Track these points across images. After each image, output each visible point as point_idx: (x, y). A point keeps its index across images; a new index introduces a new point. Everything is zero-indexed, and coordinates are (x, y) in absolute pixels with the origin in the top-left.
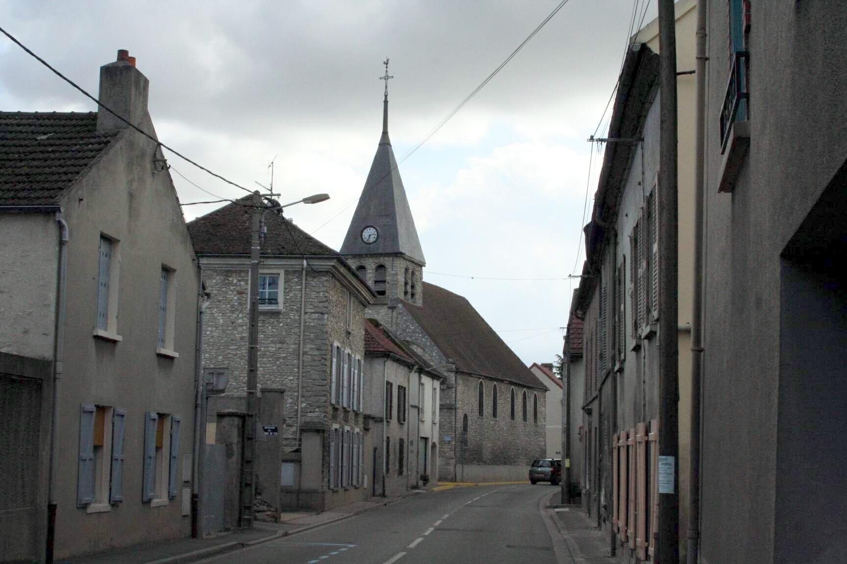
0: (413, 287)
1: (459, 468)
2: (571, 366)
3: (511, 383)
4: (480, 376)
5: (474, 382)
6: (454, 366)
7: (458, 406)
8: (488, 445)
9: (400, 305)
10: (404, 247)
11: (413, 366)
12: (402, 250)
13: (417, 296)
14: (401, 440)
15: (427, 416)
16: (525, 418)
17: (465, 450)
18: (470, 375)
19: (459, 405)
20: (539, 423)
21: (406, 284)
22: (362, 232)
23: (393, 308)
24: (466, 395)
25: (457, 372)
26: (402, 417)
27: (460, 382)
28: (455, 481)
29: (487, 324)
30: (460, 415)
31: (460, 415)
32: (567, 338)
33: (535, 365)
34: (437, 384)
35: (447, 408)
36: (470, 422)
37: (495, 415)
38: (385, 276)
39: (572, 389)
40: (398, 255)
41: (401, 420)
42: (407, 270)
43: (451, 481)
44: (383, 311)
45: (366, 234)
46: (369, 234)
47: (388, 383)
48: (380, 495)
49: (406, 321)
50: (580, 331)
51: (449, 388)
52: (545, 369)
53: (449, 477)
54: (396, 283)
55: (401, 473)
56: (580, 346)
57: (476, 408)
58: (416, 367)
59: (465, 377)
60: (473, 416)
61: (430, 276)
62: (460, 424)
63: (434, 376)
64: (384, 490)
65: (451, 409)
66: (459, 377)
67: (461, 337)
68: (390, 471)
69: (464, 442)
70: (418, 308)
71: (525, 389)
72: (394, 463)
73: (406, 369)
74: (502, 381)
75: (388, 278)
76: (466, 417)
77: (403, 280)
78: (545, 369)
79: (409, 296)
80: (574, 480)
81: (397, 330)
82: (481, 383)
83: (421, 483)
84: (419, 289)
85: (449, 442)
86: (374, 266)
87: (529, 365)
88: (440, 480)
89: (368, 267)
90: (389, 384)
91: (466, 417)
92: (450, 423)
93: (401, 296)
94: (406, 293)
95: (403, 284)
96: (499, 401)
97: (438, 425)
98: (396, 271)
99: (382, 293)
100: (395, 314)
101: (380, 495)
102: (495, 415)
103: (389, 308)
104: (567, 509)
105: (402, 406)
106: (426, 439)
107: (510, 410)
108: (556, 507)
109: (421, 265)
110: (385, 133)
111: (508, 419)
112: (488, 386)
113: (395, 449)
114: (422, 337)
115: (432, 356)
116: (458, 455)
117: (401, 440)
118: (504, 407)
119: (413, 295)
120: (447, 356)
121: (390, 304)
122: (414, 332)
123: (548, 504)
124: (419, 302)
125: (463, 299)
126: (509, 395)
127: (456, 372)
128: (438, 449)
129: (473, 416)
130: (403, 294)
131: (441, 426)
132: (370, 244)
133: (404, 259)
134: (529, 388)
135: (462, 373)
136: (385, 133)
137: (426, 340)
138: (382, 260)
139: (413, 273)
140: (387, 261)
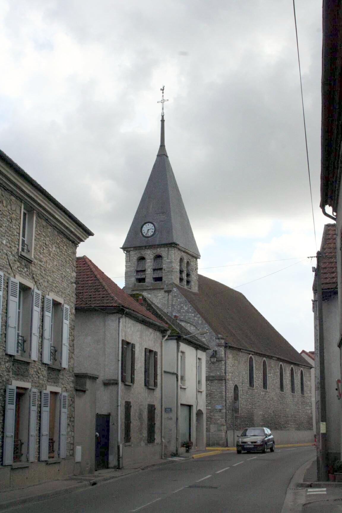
0: (188, 275)
1: (230, 433)
2: (325, 305)
3: (279, 360)
4: (249, 352)
5: (244, 358)
6: (223, 341)
7: (227, 377)
8: (259, 414)
9: (174, 289)
10: (177, 238)
11: (166, 330)
12: (175, 241)
13: (192, 283)
14: (151, 409)
15: (191, 382)
16: (293, 390)
17: (236, 418)
18: (239, 350)
19: (229, 376)
20: (306, 395)
21: (181, 272)
22: (142, 227)
23: (168, 292)
24: (235, 367)
25: (227, 347)
26: (152, 382)
27: (230, 356)
28: (227, 446)
29: (264, 318)
30: (231, 385)
31: (231, 385)
32: (317, 271)
33: (303, 351)
34: (203, 355)
35: (214, 379)
36: (240, 393)
37: (265, 386)
38: (161, 265)
39: (325, 334)
40: (173, 245)
41: (150, 384)
42: (181, 260)
43: (223, 446)
44: (161, 294)
45: (145, 228)
46: (148, 229)
47: (126, 343)
48: (114, 467)
49: (181, 303)
50: (333, 265)
51: (219, 361)
52: (311, 355)
53: (221, 442)
54: (171, 271)
55: (151, 439)
56: (334, 280)
57: (247, 380)
58: (169, 333)
59: (235, 352)
60: (244, 388)
61: (205, 268)
62: (230, 394)
63: (198, 346)
64: (119, 464)
65: (222, 380)
66: (228, 351)
67: (233, 321)
68: (133, 439)
69: (235, 410)
70: (195, 294)
71: (292, 366)
72: (140, 431)
73: (158, 334)
74: (270, 357)
75: (164, 266)
76: (236, 388)
77: (178, 268)
78: (311, 355)
79: (185, 283)
80: (333, 450)
81: (173, 311)
82: (251, 358)
83: (182, 450)
84: (193, 278)
85: (220, 411)
86: (152, 257)
87: (300, 352)
88: (208, 445)
89: (147, 257)
90: (128, 347)
91: (236, 388)
92: (221, 392)
93: (177, 282)
94: (181, 280)
95: (178, 270)
96: (268, 375)
97: (204, 394)
98: (172, 259)
99: (159, 279)
100: (170, 297)
101: (114, 467)
102: (265, 386)
103: (165, 291)
104: (323, 491)
105: (152, 371)
106: (190, 407)
107: (279, 383)
108: (310, 486)
109: (196, 256)
110: (162, 146)
111: (278, 391)
112: (258, 362)
113: (140, 414)
114: (195, 316)
115: (206, 337)
116: (229, 422)
117: (151, 409)
118: (273, 379)
119: (188, 282)
120: (217, 332)
121: (166, 289)
122: (187, 312)
123: (301, 481)
124: (195, 288)
125: (241, 294)
126: (278, 370)
127: (226, 347)
128: (205, 416)
129: (244, 388)
130: (178, 280)
131: (209, 395)
132: (148, 237)
133: (179, 249)
134: (295, 364)
135: (231, 347)
136: (162, 146)
137: (198, 319)
138: (159, 251)
139: (188, 263)
140: (163, 251)
